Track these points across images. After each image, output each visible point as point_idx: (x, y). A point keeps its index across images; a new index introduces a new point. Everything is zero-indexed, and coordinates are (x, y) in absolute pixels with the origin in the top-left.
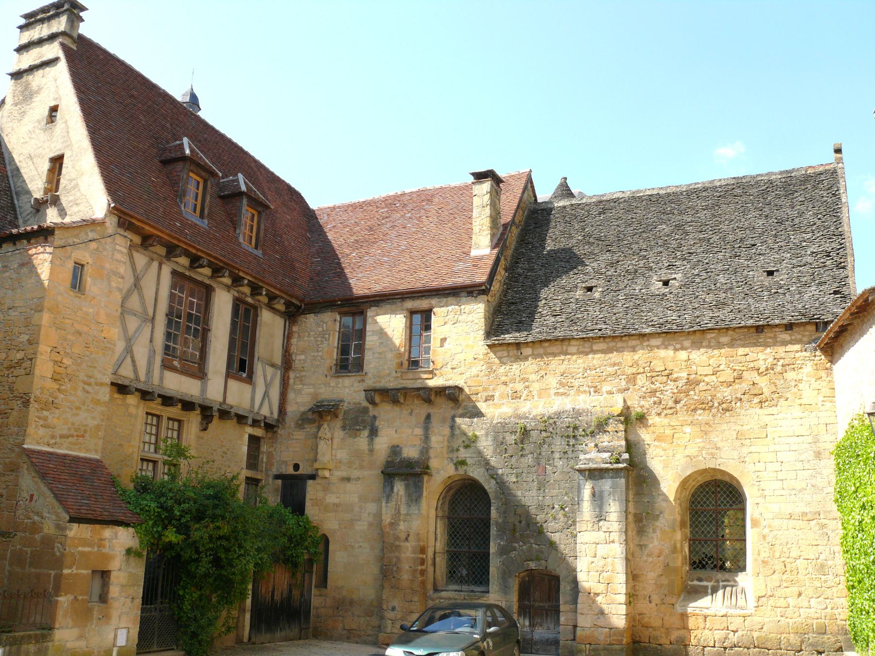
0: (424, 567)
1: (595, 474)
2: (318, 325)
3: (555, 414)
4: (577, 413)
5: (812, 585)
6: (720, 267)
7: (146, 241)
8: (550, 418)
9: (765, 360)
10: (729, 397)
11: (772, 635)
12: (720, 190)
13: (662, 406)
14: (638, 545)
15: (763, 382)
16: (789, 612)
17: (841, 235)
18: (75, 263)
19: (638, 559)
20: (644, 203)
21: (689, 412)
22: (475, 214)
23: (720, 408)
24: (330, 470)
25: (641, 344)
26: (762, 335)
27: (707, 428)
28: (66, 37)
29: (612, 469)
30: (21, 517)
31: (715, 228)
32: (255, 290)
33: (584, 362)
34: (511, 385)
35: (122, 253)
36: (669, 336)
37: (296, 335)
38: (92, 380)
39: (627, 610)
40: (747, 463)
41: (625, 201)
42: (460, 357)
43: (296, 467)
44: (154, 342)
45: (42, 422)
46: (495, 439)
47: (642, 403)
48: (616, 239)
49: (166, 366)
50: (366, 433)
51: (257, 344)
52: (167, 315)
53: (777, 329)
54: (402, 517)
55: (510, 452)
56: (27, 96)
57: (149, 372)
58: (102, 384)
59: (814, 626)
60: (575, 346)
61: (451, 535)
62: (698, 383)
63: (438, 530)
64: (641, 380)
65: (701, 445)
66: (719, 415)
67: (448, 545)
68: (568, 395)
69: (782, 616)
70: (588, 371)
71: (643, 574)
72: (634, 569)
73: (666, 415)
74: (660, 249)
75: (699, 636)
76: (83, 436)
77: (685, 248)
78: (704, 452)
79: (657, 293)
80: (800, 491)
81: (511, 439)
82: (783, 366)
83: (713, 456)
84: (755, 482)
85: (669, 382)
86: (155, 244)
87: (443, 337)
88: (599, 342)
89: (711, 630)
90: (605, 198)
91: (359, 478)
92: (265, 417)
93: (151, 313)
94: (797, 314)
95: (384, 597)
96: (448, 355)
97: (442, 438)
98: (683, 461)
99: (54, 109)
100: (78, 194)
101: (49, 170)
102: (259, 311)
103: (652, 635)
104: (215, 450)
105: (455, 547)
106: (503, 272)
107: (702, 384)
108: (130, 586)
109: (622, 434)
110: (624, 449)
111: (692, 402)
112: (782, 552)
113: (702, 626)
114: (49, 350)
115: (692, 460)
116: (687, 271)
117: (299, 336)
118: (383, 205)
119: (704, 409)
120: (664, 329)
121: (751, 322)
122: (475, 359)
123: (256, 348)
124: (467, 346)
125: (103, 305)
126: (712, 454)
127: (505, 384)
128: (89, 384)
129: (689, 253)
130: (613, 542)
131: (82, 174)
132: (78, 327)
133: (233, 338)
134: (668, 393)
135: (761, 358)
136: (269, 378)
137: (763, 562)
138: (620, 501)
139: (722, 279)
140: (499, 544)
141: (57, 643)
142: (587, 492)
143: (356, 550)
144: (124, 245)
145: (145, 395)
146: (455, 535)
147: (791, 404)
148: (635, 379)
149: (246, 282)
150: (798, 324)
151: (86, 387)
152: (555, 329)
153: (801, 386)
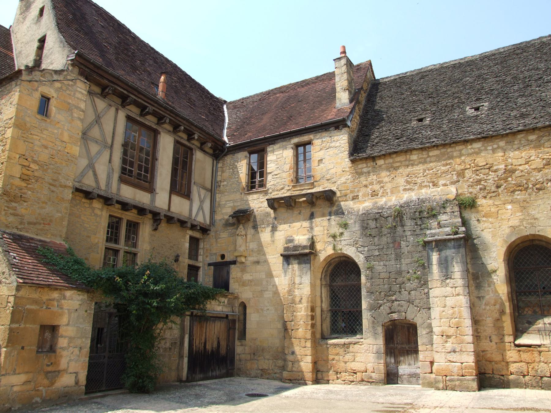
0: (314, 322)
3: (405, 203)
6: (517, 94)
10: (541, 180)
13: (486, 191)
18: (42, 96)
19: (477, 308)
20: (450, 69)
23: (535, 188)
25: (466, 148)
32: (190, 137)
34: (370, 187)
35: (82, 94)
36: (487, 140)
37: (219, 169)
38: (57, 183)
42: (332, 171)
44: (113, 163)
45: (11, 211)
47: (471, 190)
48: (435, 90)
49: (122, 180)
50: (269, 229)
51: (193, 174)
52: (123, 145)
54: (296, 286)
57: (108, 184)
58: (65, 186)
60: (415, 154)
61: (332, 299)
62: (513, 171)
63: (323, 295)
64: (468, 174)
65: (522, 217)
66: (534, 193)
67: (330, 305)
68: (414, 190)
70: (427, 172)
71: (483, 320)
72: (476, 316)
73: (491, 197)
75: (536, 367)
76: (49, 224)
78: (524, 223)
83: (532, 225)
87: (320, 159)
93: (109, 141)
96: (325, 170)
98: (508, 231)
102: (194, 151)
103: (494, 368)
110: (461, 224)
111: (510, 186)
114: (18, 156)
115: (515, 229)
119: (521, 190)
123: (193, 176)
125: (66, 129)
126: (531, 223)
127: (366, 186)
133: (175, 168)
134: (490, 181)
136: (202, 197)
139: (520, 101)
140: (369, 302)
142: (435, 257)
143: (265, 312)
144: (84, 88)
145: (107, 201)
146: (336, 298)
149: (182, 128)
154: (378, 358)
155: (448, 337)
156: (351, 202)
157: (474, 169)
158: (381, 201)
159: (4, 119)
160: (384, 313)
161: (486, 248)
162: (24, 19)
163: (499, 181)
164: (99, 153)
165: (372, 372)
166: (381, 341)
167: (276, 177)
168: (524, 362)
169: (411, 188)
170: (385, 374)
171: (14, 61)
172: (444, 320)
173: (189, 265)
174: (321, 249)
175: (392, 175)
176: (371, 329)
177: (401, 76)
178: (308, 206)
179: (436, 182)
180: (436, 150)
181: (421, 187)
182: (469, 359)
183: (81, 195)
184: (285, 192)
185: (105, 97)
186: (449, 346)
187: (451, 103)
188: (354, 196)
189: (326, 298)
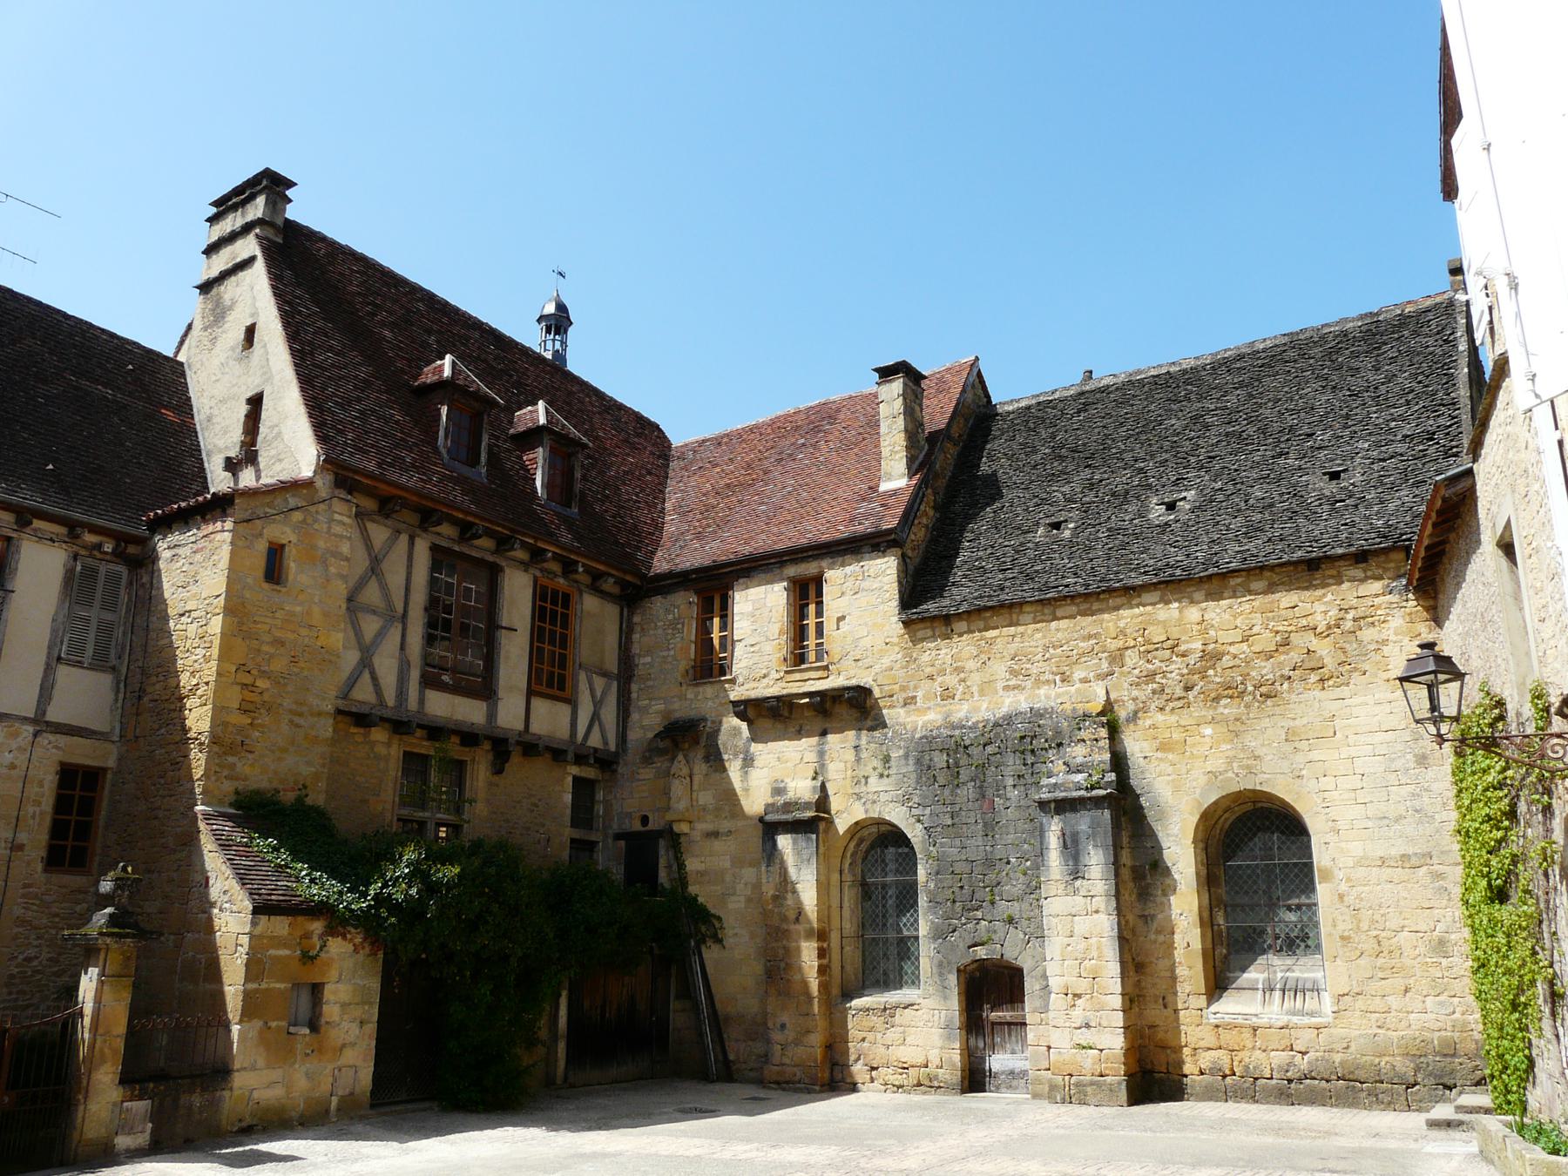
0: (825, 962)
1: (1064, 806)
2: (668, 611)
3: (1004, 718)
4: (1036, 714)
5: (1426, 974)
7: (387, 506)
8: (996, 725)
9: (1325, 612)
10: (1271, 676)
11: (1365, 1058)
12: (1263, 355)
14: (1140, 916)
15: (1323, 648)
16: (1391, 1019)
17: (1454, 404)
19: (1142, 939)
20: (1146, 389)
21: (1209, 704)
22: (883, 429)
23: (1258, 693)
24: (690, 822)
28: (265, 227)
29: (1090, 798)
30: (195, 911)
31: (1253, 414)
33: (1044, 637)
35: (344, 524)
37: (638, 628)
38: (305, 709)
39: (1125, 1020)
40: (1305, 780)
41: (1117, 389)
42: (866, 642)
43: (645, 820)
44: (407, 651)
45: (225, 773)
46: (918, 762)
47: (1135, 693)
49: (430, 681)
52: (426, 609)
53: (1342, 563)
55: (941, 780)
56: (218, 315)
58: (319, 714)
59: (1436, 1042)
60: (1028, 613)
62: (1217, 656)
63: (846, 904)
64: (1131, 658)
65: (1230, 753)
66: (1257, 704)
68: (1023, 689)
69: (1379, 1027)
70: (1051, 650)
71: (1151, 962)
72: (1138, 955)
73: (1173, 709)
74: (1165, 456)
75: (1247, 1060)
77: (1203, 450)
78: (1235, 765)
79: (1157, 522)
80: (1397, 820)
81: (940, 760)
82: (1355, 620)
84: (1319, 809)
85: (1174, 658)
86: (398, 508)
87: (840, 615)
88: (1065, 605)
89: (1264, 1051)
92: (596, 750)
93: (399, 607)
96: (849, 640)
98: (1203, 780)
99: (250, 332)
100: (281, 446)
101: (246, 416)
103: (1171, 1061)
104: (519, 802)
106: (931, 513)
107: (1226, 658)
108: (357, 1004)
109: (1105, 743)
110: (1107, 767)
111: (1211, 686)
112: (1373, 921)
115: (1216, 777)
116: (1205, 485)
117: (643, 629)
118: (769, 431)
119: (1231, 697)
120: (1162, 577)
122: (887, 644)
126: (1248, 767)
127: (931, 677)
128: (301, 715)
129: (1210, 457)
130: (1097, 912)
131: (287, 417)
132: (278, 634)
134: (1174, 674)
135: (1319, 611)
136: (599, 694)
137: (1342, 938)
140: (932, 923)
141: (236, 1093)
142: (1053, 841)
145: (399, 726)
147: (1373, 680)
150: (1376, 550)
151: (296, 719)
152: (1002, 589)
153: (1386, 650)
154: (949, 1038)
155: (1077, 996)
156: (902, 711)
157: (1142, 649)
158: (959, 711)
159: (203, 596)
160: (961, 945)
161: (1162, 816)
162: (213, 341)
163: (1190, 676)
164: (381, 634)
165: (937, 1067)
166: (954, 1003)
167: (752, 649)
168: (1225, 1049)
169: (1020, 686)
170: (963, 1071)
171: (197, 437)
172: (1071, 962)
173: (573, 841)
174: (840, 808)
175: (982, 656)
176: (936, 978)
177: (1041, 399)
178: (816, 716)
179: (1068, 673)
180: (1069, 605)
181: (1038, 683)
182: (1115, 1042)
183: (347, 719)
184: (771, 683)
185: (387, 516)
186: (1078, 1015)
187: (1126, 487)
188: (908, 698)
189: (852, 911)
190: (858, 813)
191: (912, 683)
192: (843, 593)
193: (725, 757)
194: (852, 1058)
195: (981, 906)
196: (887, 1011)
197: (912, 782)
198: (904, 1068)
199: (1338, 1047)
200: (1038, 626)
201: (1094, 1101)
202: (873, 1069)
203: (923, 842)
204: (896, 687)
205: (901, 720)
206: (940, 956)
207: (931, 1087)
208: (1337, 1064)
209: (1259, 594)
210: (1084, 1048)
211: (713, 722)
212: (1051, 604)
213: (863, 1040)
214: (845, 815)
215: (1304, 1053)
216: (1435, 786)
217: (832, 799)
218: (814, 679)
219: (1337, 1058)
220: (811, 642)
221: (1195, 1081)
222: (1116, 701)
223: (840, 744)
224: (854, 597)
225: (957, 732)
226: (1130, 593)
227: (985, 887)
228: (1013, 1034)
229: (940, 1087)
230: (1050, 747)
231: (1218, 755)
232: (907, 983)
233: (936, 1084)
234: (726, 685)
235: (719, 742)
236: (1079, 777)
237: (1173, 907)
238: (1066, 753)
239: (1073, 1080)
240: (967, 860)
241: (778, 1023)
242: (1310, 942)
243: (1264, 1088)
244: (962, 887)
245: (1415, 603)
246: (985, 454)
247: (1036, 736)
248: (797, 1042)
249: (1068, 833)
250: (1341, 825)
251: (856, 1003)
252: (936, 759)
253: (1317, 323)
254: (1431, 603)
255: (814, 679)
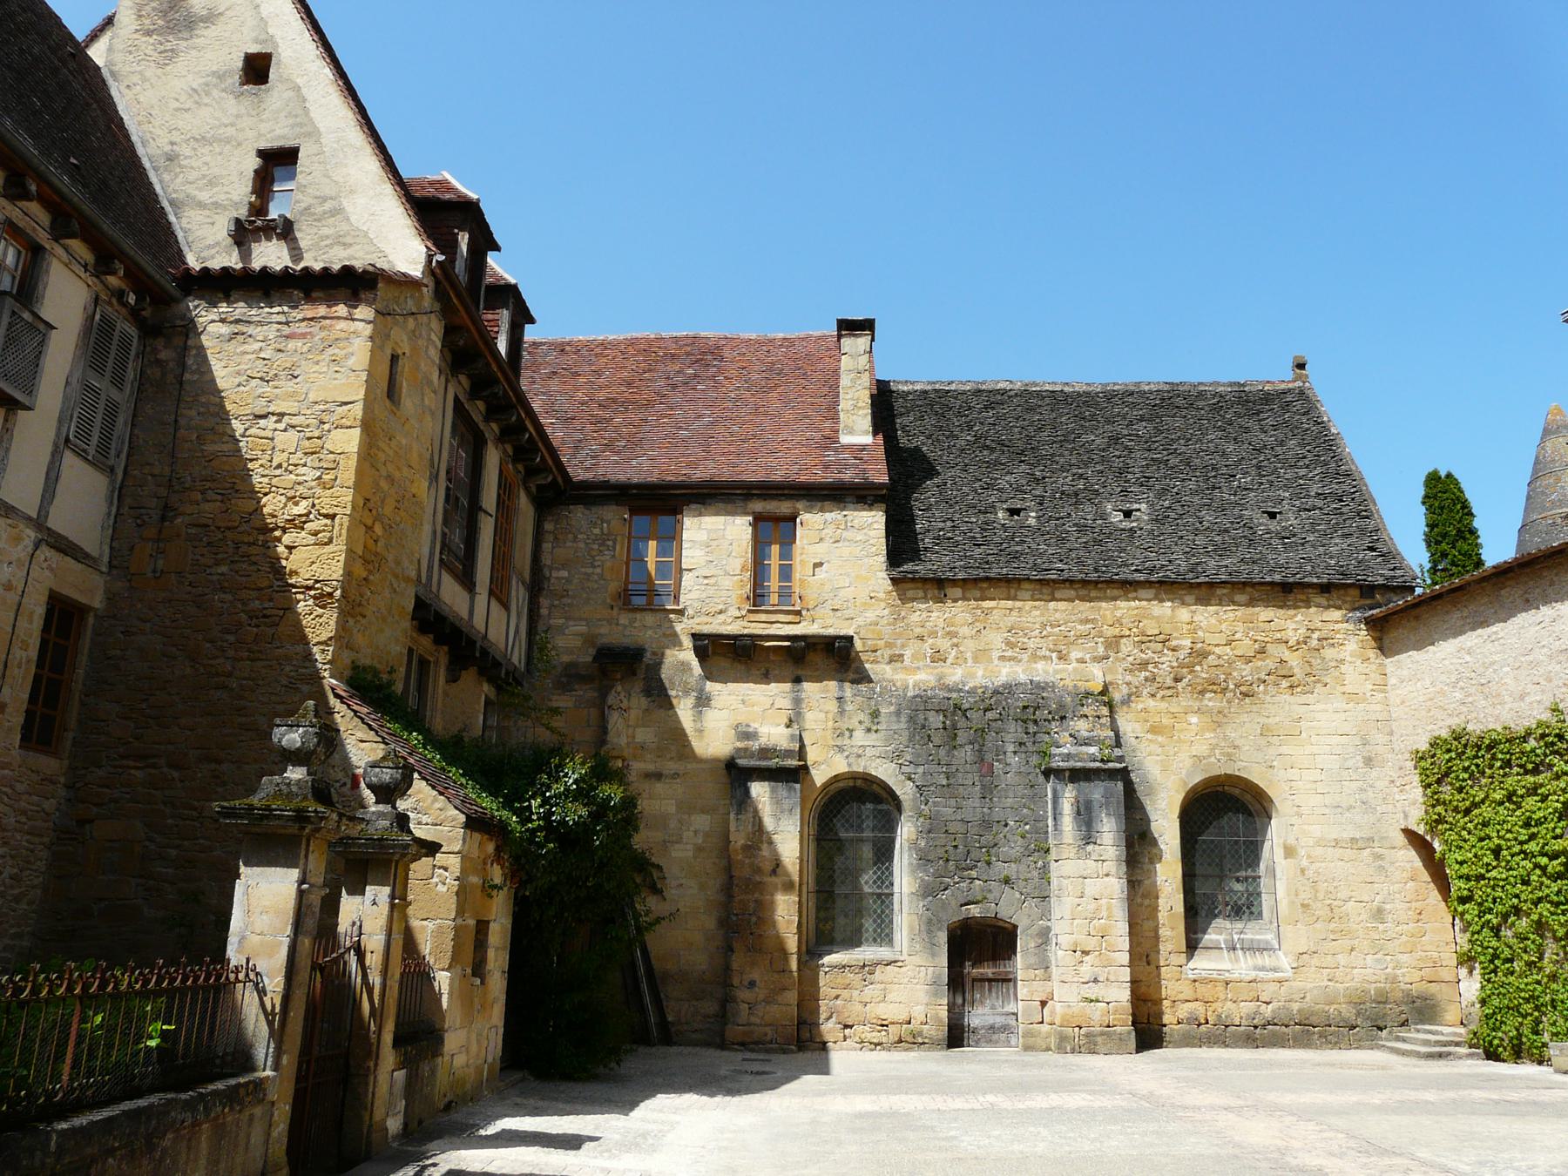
4: (1038, 687)
8: (996, 692)
9: (1296, 630)
15: (1294, 661)
16: (1339, 973)
26: (1291, 597)
27: (1220, 718)
41: (1016, 394)
47: (1129, 678)
53: (1310, 591)
59: (1372, 992)
60: (1027, 590)
62: (1204, 655)
64: (1126, 646)
65: (1214, 741)
66: (1237, 701)
68: (1020, 661)
69: (1329, 980)
70: (1048, 628)
73: (1163, 697)
81: (936, 720)
85: (1166, 651)
90: (984, 387)
91: (678, 775)
94: (1333, 572)
95: (735, 966)
96: (827, 587)
97: (822, 715)
98: (1188, 763)
101: (255, 171)
105: (879, 887)
111: (1198, 680)
113: (1222, 997)
115: (1201, 761)
117: (556, 538)
119: (1215, 692)
120: (1154, 577)
121: (1277, 577)
124: (857, 577)
126: (1229, 754)
127: (921, 638)
130: (1107, 875)
134: (1164, 666)
137: (1303, 905)
138: (1118, 817)
148: (1118, 644)
154: (936, 994)
156: (888, 668)
157: (1136, 639)
158: (954, 674)
159: (312, 397)
161: (1151, 792)
165: (921, 1024)
167: (706, 581)
175: (978, 624)
176: (924, 936)
177: (937, 387)
179: (1064, 652)
181: (1035, 657)
186: (1086, 970)
188: (895, 655)
190: (840, 766)
191: (899, 641)
192: (821, 539)
193: (672, 693)
194: (823, 1017)
195: (976, 866)
196: (867, 968)
197: (904, 739)
198: (883, 1025)
199: (1296, 997)
200: (1037, 603)
201: (1104, 1049)
202: (846, 1027)
203: (914, 799)
204: (881, 643)
205: (887, 676)
206: (929, 913)
207: (915, 1043)
208: (1295, 1012)
209: (1242, 606)
210: (1092, 1001)
211: (654, 653)
212: (1048, 586)
213: (837, 997)
214: (823, 767)
215: (1268, 1003)
216: (1378, 784)
217: (808, 749)
218: (782, 623)
219: (1295, 1007)
220: (774, 583)
221: (1172, 1030)
222: (1111, 683)
223: (820, 695)
224: (836, 545)
225: (954, 695)
226: (1128, 587)
227: (981, 848)
228: (994, 990)
229: (924, 1043)
230: (1053, 719)
231: (1202, 741)
232: (867, 940)
233: (920, 1040)
234: (672, 616)
235: (663, 676)
236: (1093, 750)
237: (1159, 874)
238: (1069, 726)
239: (1083, 1031)
240: (962, 820)
241: (747, 979)
242: (1253, 909)
243: (1234, 1035)
244: (956, 847)
245: (1366, 633)
246: (898, 426)
247: (1039, 707)
248: (768, 1001)
249: (1081, 801)
250: (1304, 810)
251: (827, 960)
252: (931, 719)
253: (1195, 380)
254: (1378, 634)
255: (782, 623)
